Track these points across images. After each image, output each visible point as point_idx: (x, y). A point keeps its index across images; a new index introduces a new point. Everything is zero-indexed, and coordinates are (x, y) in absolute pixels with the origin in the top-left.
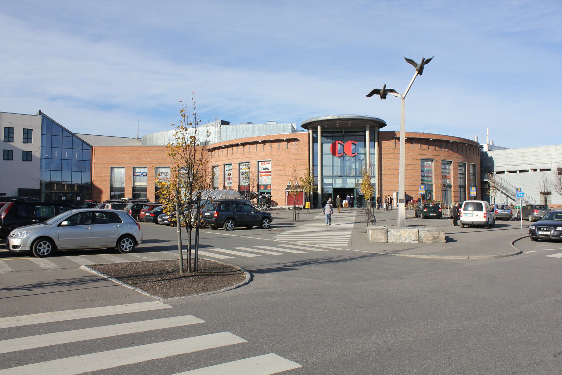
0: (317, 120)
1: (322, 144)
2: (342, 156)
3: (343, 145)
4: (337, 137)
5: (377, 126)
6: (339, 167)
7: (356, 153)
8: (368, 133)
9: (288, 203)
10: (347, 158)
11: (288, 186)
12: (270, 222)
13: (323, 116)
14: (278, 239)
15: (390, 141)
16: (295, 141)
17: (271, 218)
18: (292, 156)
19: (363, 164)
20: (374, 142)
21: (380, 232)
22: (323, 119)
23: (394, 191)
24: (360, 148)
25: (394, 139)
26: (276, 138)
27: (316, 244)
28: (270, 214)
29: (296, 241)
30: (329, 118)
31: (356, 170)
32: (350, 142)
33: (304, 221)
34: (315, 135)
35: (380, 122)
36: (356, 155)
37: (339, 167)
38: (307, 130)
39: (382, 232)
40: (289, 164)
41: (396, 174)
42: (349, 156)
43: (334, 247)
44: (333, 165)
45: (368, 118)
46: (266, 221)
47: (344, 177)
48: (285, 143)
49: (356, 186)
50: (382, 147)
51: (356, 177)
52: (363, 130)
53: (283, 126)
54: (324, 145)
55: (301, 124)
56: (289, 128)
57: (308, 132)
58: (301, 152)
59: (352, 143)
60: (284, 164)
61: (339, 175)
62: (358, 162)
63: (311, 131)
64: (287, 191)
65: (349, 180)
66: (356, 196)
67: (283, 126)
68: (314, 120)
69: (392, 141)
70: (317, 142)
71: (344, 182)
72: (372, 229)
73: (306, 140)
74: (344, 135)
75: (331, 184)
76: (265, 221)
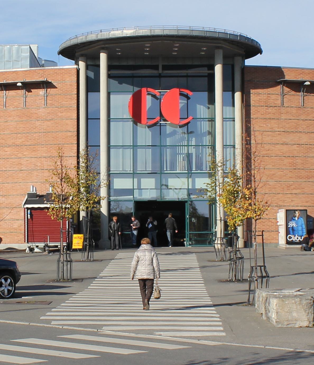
0: (100, 37)
1: (109, 94)
2: (155, 124)
3: (157, 98)
4: (143, 79)
5: (239, 55)
6: (149, 151)
7: (190, 118)
8: (218, 69)
9: (30, 237)
10: (169, 129)
11: (30, 195)
12: (16, 283)
13: (113, 30)
14: (53, 323)
15: (270, 90)
16: (44, 88)
17: (16, 275)
18: (38, 123)
19: (206, 143)
20: (231, 93)
21: (296, 303)
22: (114, 37)
23: (280, 207)
24: (198, 106)
25: (279, 85)
26: (37, 79)
27: (151, 332)
28: (14, 264)
29: (101, 326)
30: (128, 32)
31: (189, 156)
32: (176, 91)
33: (82, 280)
34: (91, 75)
35: (248, 44)
36: (189, 123)
37: (149, 151)
38: (74, 62)
39: (300, 304)
40: (29, 143)
41: (284, 168)
42: (172, 125)
43: (199, 338)
44: (135, 147)
45: (221, 36)
46: (6, 280)
47: (161, 173)
48: (19, 92)
49: (189, 195)
50: (252, 103)
51: (189, 174)
52: (205, 63)
53: (10, 51)
54: (112, 96)
55: (58, 49)
56: (23, 54)
57: (76, 66)
58: (60, 114)
59: (181, 94)
60: (19, 142)
61: (149, 169)
62: (194, 139)
63: (82, 65)
64: (28, 209)
65: (173, 182)
66: (191, 221)
67: (10, 51)
68: (92, 37)
69: (275, 88)
70: (99, 92)
71: (162, 186)
72: (275, 297)
73: (71, 85)
74: (160, 74)
75: (130, 192)
76: (3, 281)
